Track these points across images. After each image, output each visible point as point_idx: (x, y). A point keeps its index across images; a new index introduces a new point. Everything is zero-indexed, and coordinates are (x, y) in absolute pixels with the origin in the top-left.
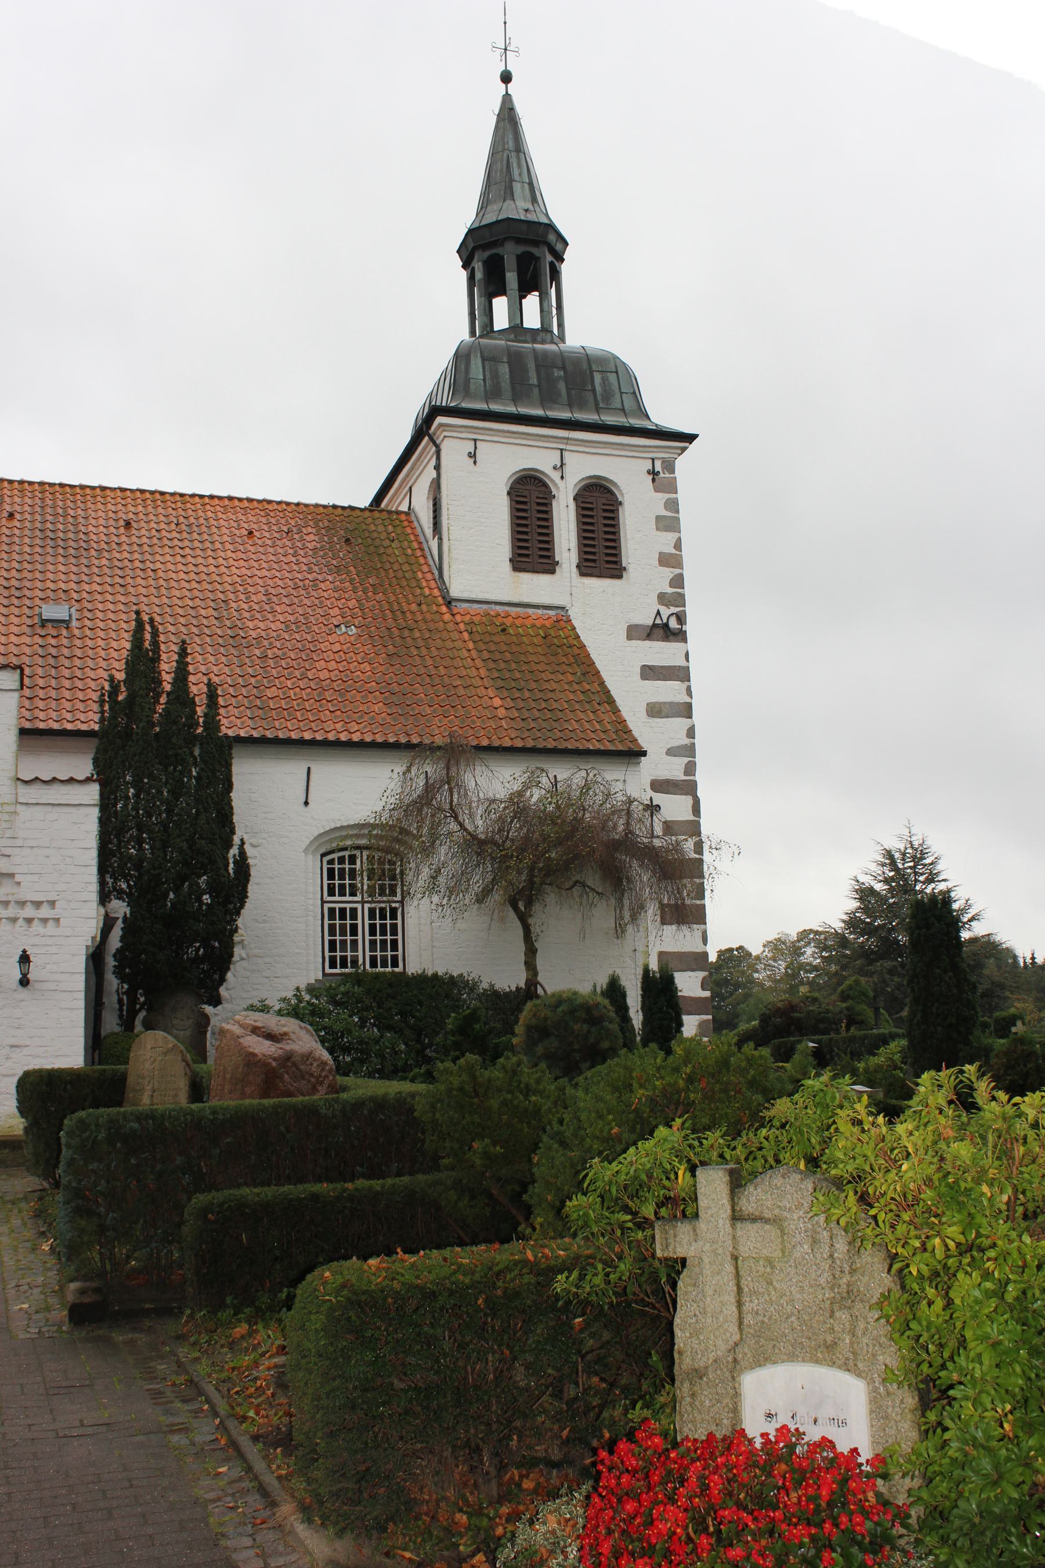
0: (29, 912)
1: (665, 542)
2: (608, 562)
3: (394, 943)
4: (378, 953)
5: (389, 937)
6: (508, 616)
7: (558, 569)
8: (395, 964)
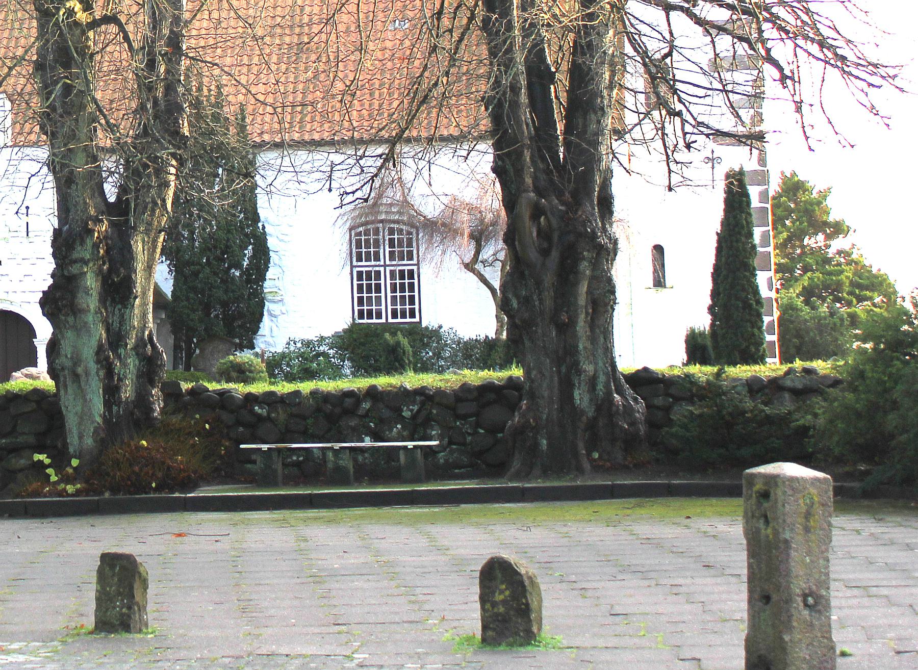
3: (412, 299)
4: (399, 307)
5: (407, 294)
8: (412, 315)
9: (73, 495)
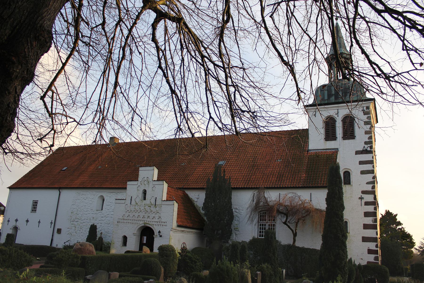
0: (163, 224)
2: (350, 135)
6: (327, 152)
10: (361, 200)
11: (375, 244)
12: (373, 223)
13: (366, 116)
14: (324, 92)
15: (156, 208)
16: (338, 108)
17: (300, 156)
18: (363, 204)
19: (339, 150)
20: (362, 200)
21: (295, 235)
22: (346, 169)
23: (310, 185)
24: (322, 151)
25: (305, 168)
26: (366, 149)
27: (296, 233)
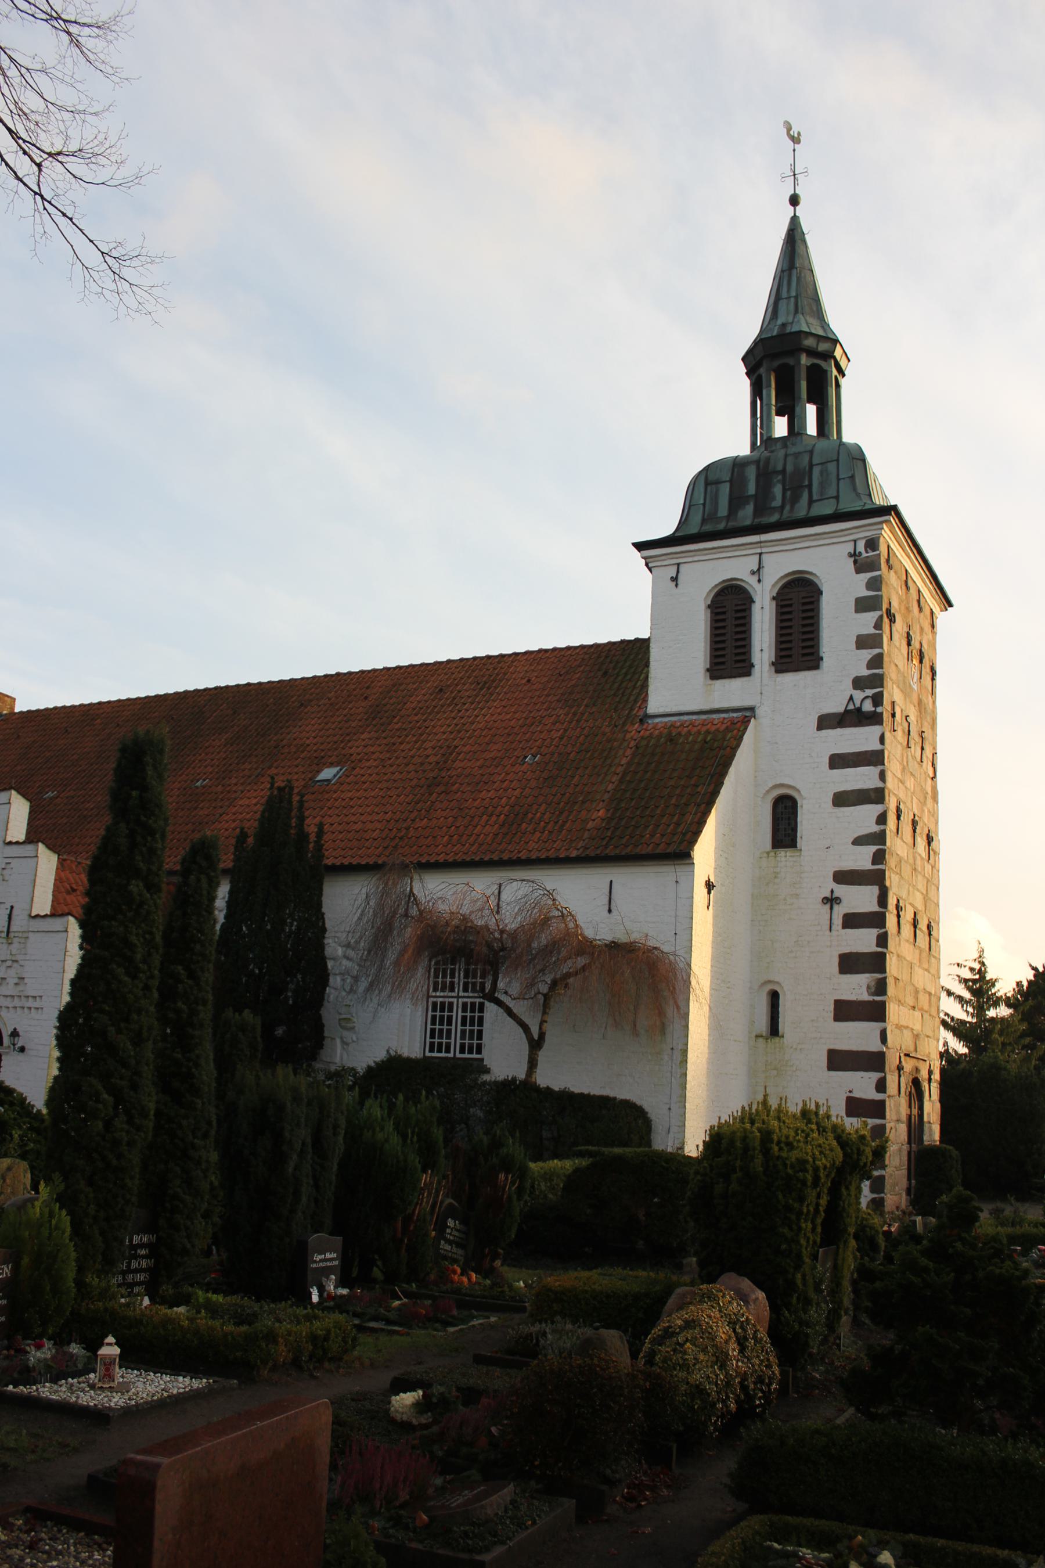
0: (31, 1003)
1: (866, 622)
2: (804, 655)
7: (773, 669)
8: (479, 1052)
9: (882, 523)
10: (831, 908)
11: (875, 1076)
12: (871, 998)
13: (866, 576)
14: (717, 491)
15: (12, 947)
16: (759, 551)
17: (609, 741)
18: (838, 921)
19: (757, 711)
20: (836, 907)
21: (536, 1044)
22: (782, 785)
23: (610, 851)
24: (694, 717)
25: (611, 787)
26: (858, 705)
27: (542, 1035)
